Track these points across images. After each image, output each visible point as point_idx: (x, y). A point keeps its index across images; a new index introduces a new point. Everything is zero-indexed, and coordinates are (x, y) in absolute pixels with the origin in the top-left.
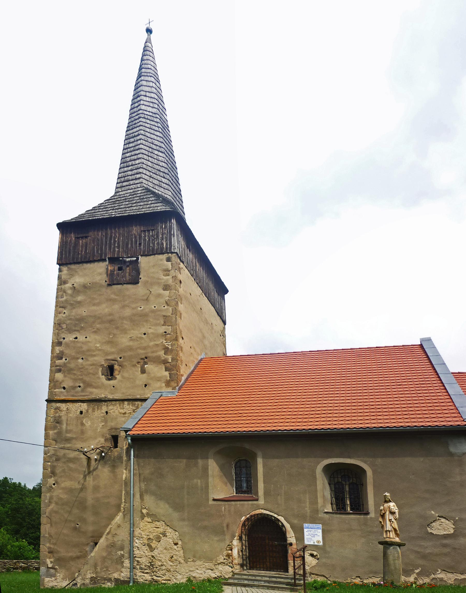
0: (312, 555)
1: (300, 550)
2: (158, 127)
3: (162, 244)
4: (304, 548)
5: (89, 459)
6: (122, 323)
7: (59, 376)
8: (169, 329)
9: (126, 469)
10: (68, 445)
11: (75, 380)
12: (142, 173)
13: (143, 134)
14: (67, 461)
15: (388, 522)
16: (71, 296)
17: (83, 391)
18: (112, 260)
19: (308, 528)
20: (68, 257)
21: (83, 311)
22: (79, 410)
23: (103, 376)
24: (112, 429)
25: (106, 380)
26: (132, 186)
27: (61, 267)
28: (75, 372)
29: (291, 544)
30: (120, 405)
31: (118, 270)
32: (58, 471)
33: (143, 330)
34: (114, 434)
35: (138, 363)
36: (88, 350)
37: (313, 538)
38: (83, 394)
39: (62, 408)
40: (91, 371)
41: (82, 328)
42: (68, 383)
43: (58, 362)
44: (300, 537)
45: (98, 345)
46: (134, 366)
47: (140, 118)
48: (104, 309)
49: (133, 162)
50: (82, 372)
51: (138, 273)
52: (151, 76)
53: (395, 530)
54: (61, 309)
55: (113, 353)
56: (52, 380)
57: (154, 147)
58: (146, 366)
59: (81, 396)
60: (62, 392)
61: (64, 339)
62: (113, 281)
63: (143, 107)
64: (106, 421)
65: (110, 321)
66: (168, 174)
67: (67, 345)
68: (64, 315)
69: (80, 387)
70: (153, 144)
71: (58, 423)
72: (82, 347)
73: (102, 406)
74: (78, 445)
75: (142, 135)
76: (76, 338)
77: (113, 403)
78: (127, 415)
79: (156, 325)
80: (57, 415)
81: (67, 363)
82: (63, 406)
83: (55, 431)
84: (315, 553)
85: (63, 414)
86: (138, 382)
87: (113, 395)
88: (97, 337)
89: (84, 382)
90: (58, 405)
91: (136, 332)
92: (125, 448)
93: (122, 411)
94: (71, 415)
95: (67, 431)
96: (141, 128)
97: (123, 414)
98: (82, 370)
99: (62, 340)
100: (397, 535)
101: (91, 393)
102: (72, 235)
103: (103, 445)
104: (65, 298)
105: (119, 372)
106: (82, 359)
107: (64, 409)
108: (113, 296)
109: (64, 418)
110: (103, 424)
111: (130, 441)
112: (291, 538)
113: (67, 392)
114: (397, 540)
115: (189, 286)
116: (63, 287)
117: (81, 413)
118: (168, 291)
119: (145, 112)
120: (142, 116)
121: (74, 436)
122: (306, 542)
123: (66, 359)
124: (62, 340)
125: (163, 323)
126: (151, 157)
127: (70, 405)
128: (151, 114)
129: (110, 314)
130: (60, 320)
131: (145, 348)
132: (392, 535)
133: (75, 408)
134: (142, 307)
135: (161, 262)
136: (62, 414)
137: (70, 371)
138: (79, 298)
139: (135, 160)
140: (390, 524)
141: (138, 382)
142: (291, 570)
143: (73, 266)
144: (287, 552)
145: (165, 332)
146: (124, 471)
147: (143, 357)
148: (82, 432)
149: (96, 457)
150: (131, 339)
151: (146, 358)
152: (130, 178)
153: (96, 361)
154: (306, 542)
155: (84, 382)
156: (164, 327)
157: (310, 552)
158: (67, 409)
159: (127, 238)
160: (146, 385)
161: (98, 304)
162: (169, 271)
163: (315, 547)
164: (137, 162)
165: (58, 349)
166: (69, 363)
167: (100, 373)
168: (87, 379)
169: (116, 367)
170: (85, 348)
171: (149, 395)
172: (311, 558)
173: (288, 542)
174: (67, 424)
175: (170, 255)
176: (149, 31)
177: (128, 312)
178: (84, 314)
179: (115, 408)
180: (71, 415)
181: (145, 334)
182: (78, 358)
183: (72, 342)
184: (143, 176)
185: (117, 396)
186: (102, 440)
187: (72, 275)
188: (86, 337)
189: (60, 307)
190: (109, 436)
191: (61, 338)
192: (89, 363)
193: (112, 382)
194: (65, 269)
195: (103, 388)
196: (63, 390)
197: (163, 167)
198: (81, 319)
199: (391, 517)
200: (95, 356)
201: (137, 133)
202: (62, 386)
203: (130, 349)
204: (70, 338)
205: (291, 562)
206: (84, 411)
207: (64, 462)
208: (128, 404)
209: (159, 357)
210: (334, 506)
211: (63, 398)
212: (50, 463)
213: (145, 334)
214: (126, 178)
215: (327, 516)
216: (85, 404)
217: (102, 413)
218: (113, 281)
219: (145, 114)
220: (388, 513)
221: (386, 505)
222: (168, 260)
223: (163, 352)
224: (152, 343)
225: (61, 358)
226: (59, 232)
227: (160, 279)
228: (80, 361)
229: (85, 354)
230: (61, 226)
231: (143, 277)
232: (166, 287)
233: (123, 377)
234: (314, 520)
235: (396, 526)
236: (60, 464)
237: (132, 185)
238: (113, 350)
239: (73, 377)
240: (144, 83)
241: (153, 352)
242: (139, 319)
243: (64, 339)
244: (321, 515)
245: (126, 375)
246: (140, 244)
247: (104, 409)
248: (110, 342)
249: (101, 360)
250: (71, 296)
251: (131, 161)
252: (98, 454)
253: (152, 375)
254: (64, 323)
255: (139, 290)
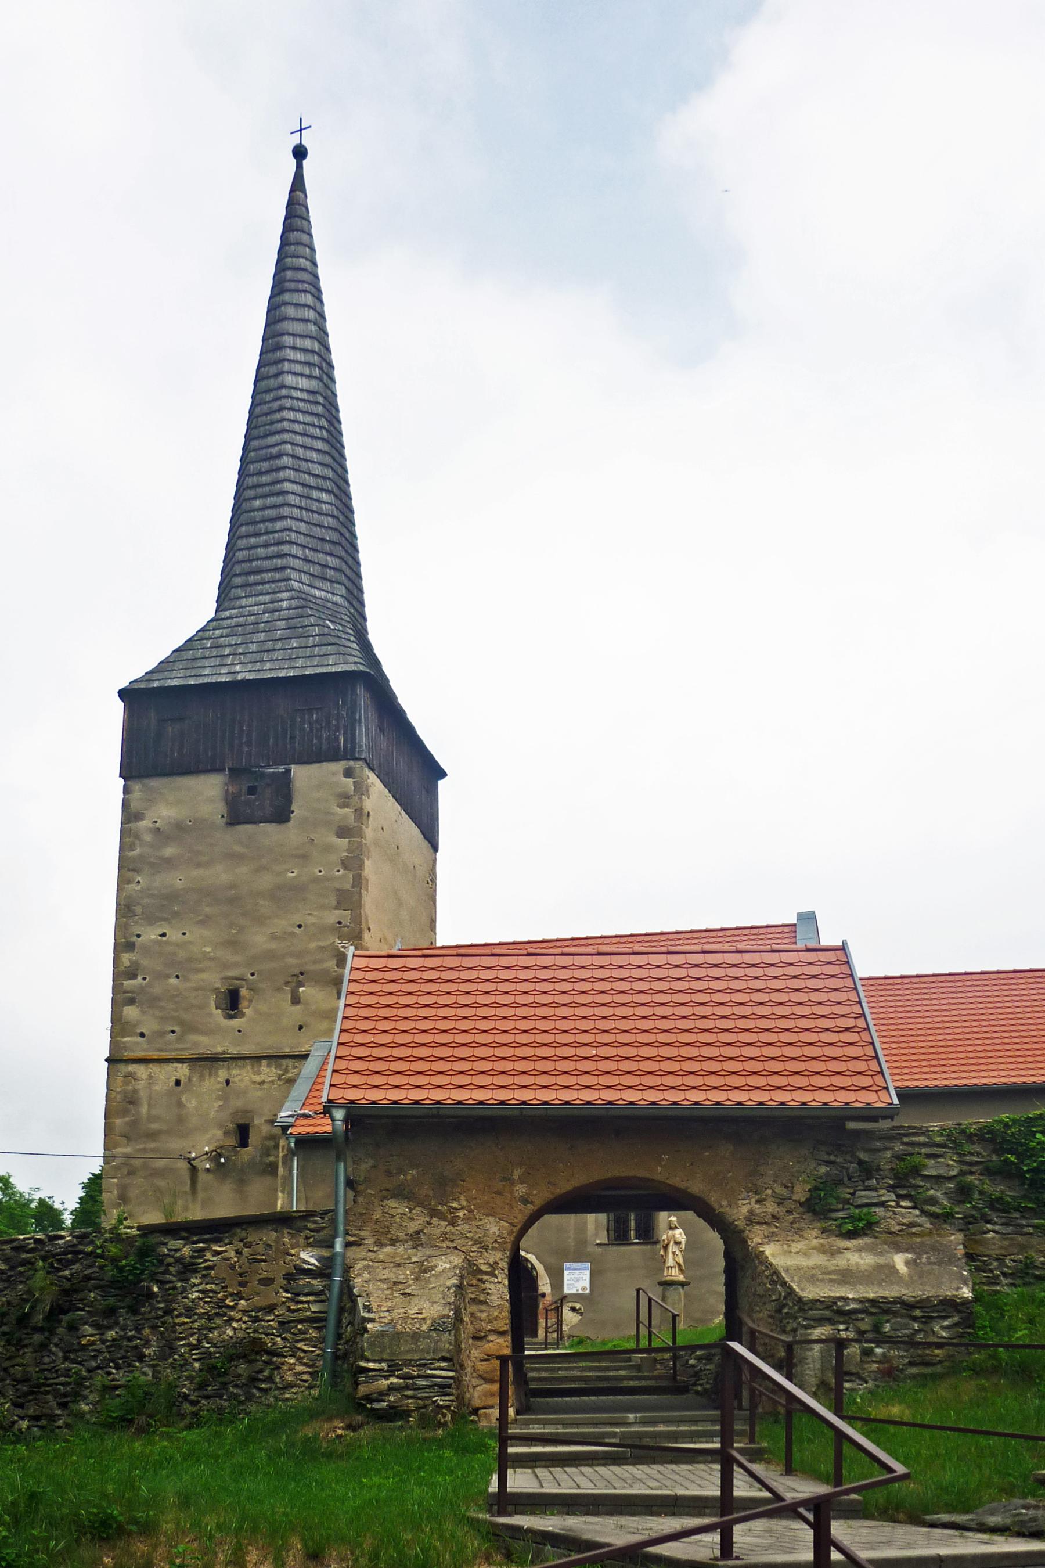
0: (573, 1309)
1: (556, 1302)
2: (321, 427)
3: (337, 739)
4: (564, 1299)
5: (194, 1170)
6: (257, 904)
7: (131, 1012)
8: (345, 916)
9: (283, 1192)
10: (153, 1145)
11: (163, 1019)
12: (290, 555)
13: (291, 452)
14: (151, 1175)
15: (671, 1255)
16: (152, 846)
17: (180, 1040)
18: (235, 773)
19: (569, 1269)
20: (140, 761)
21: (177, 880)
22: (174, 1079)
23: (219, 1011)
24: (237, 1112)
25: (225, 1018)
26: (267, 586)
27: (129, 783)
28: (162, 1004)
29: (544, 1295)
30: (253, 1068)
31: (249, 794)
32: (133, 1193)
33: (297, 919)
34: (241, 1122)
35: (287, 983)
36: (190, 960)
37: (576, 1284)
38: (180, 1046)
39: (139, 1074)
40: (194, 1002)
41: (176, 914)
42: (149, 1026)
43: (128, 984)
44: (557, 1281)
45: (208, 949)
46: (279, 989)
47: (281, 409)
48: (220, 875)
49: (269, 525)
50: (176, 1002)
51: (288, 798)
52: (305, 291)
53: (679, 1265)
54: (130, 874)
55: (236, 965)
56: (116, 1018)
57: (311, 481)
58: (301, 989)
59: (177, 1050)
60: (138, 1043)
61: (139, 936)
62: (237, 815)
63: (289, 380)
64: (225, 1097)
65: (233, 901)
66: (340, 544)
67: (146, 950)
68: (139, 888)
69: (173, 1032)
70: (309, 474)
71: (131, 1103)
72: (175, 954)
73: (217, 1069)
74: (175, 1145)
75: (288, 455)
76: (164, 935)
77: (240, 1063)
78: (266, 1086)
79: (323, 907)
80: (130, 1088)
81: (146, 985)
82: (141, 1071)
83: (127, 1119)
84: (578, 1306)
85: (141, 1085)
86: (285, 1021)
87: (238, 1048)
88: (206, 933)
89: (182, 1023)
90: (132, 1068)
91: (284, 922)
92: (281, 1155)
93: (258, 1078)
94: (157, 1088)
95: (151, 1119)
96: (286, 436)
97: (259, 1084)
98: (176, 999)
99: (134, 939)
100: (681, 1270)
101: (196, 1044)
102: (152, 714)
103: (221, 1143)
104: (138, 851)
105: (251, 1001)
106: (177, 977)
107: (144, 1077)
108: (237, 848)
109: (143, 1094)
110: (220, 1103)
111: (293, 1145)
112: (545, 1286)
113: (149, 1042)
114: (681, 1278)
115: (378, 799)
116: (132, 825)
117: (178, 1083)
118: (347, 840)
119: (294, 394)
120: (288, 405)
121: (164, 1127)
122: (567, 1291)
123: (144, 979)
124: (134, 939)
125: (334, 903)
126: (306, 509)
127: (154, 1068)
128: (304, 396)
129: (233, 886)
130: (129, 897)
131: (299, 955)
132: (675, 1272)
133: (165, 1075)
134: (296, 871)
135: (334, 779)
136: (140, 1087)
137: (153, 1002)
138: (169, 851)
139: (272, 520)
140: (674, 1257)
141: (285, 1021)
142: (541, 1333)
143: (155, 783)
144: (537, 1306)
145: (340, 923)
146: (280, 1194)
147: (297, 971)
148: (181, 1120)
149: (208, 1166)
150: (273, 937)
151: (302, 974)
152: (266, 564)
153: (202, 980)
154: (567, 1291)
155: (182, 1023)
156: (337, 912)
157: (570, 1304)
158: (150, 1076)
159: (267, 723)
160: (301, 1028)
161: (207, 865)
162: (348, 797)
163: (578, 1297)
164: (279, 525)
165: (126, 958)
166: (149, 985)
167: (213, 1005)
168: (186, 1016)
169: (244, 992)
170: (182, 954)
171: (307, 1047)
172: (571, 1314)
173: (540, 1292)
174: (149, 1105)
175: (351, 763)
176: (300, 153)
177: (266, 881)
178: (179, 884)
179: (244, 1072)
180: (157, 1088)
181: (300, 926)
182: (168, 976)
183: (156, 942)
184: (292, 562)
185: (246, 1050)
186: (219, 1133)
187: (151, 801)
188: (184, 934)
189: (129, 870)
190: (231, 1126)
191: (132, 935)
192: (188, 985)
193: (236, 1022)
194: (136, 787)
195: (221, 1034)
196: (140, 1039)
197: (331, 528)
198: (172, 896)
199: (676, 1249)
200: (202, 970)
201: (277, 449)
202: (139, 1031)
203: (270, 955)
204: (151, 934)
205: (542, 1322)
206: (183, 1079)
207: (145, 1178)
208: (269, 1066)
209: (326, 972)
210: (612, 1233)
211: (140, 1054)
212: (115, 1180)
213: (300, 926)
214: (254, 564)
215: (599, 1250)
216: (185, 1065)
217: (219, 1083)
218: (237, 815)
219: (292, 398)
220: (672, 1243)
221: (670, 1232)
222: (348, 773)
223: (335, 962)
224: (313, 945)
225: (134, 977)
226: (122, 704)
227: (333, 814)
228: (173, 981)
229: (182, 966)
230: (123, 694)
231: (298, 809)
232: (343, 832)
233: (257, 1011)
234: (578, 1257)
235: (681, 1261)
236: (138, 1181)
237: (268, 582)
238: (237, 958)
239: (158, 1013)
240: (291, 311)
241: (315, 962)
242: (287, 894)
243: (139, 936)
244: (590, 1249)
245: (263, 1007)
246: (292, 738)
247: (223, 1074)
248: (232, 944)
249: (214, 979)
250: (152, 846)
251: (263, 521)
252: (210, 1160)
253: (313, 1007)
254: (139, 904)
255: (289, 835)
